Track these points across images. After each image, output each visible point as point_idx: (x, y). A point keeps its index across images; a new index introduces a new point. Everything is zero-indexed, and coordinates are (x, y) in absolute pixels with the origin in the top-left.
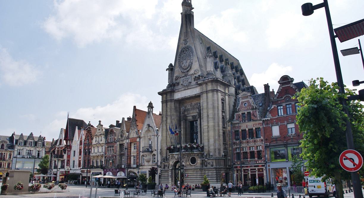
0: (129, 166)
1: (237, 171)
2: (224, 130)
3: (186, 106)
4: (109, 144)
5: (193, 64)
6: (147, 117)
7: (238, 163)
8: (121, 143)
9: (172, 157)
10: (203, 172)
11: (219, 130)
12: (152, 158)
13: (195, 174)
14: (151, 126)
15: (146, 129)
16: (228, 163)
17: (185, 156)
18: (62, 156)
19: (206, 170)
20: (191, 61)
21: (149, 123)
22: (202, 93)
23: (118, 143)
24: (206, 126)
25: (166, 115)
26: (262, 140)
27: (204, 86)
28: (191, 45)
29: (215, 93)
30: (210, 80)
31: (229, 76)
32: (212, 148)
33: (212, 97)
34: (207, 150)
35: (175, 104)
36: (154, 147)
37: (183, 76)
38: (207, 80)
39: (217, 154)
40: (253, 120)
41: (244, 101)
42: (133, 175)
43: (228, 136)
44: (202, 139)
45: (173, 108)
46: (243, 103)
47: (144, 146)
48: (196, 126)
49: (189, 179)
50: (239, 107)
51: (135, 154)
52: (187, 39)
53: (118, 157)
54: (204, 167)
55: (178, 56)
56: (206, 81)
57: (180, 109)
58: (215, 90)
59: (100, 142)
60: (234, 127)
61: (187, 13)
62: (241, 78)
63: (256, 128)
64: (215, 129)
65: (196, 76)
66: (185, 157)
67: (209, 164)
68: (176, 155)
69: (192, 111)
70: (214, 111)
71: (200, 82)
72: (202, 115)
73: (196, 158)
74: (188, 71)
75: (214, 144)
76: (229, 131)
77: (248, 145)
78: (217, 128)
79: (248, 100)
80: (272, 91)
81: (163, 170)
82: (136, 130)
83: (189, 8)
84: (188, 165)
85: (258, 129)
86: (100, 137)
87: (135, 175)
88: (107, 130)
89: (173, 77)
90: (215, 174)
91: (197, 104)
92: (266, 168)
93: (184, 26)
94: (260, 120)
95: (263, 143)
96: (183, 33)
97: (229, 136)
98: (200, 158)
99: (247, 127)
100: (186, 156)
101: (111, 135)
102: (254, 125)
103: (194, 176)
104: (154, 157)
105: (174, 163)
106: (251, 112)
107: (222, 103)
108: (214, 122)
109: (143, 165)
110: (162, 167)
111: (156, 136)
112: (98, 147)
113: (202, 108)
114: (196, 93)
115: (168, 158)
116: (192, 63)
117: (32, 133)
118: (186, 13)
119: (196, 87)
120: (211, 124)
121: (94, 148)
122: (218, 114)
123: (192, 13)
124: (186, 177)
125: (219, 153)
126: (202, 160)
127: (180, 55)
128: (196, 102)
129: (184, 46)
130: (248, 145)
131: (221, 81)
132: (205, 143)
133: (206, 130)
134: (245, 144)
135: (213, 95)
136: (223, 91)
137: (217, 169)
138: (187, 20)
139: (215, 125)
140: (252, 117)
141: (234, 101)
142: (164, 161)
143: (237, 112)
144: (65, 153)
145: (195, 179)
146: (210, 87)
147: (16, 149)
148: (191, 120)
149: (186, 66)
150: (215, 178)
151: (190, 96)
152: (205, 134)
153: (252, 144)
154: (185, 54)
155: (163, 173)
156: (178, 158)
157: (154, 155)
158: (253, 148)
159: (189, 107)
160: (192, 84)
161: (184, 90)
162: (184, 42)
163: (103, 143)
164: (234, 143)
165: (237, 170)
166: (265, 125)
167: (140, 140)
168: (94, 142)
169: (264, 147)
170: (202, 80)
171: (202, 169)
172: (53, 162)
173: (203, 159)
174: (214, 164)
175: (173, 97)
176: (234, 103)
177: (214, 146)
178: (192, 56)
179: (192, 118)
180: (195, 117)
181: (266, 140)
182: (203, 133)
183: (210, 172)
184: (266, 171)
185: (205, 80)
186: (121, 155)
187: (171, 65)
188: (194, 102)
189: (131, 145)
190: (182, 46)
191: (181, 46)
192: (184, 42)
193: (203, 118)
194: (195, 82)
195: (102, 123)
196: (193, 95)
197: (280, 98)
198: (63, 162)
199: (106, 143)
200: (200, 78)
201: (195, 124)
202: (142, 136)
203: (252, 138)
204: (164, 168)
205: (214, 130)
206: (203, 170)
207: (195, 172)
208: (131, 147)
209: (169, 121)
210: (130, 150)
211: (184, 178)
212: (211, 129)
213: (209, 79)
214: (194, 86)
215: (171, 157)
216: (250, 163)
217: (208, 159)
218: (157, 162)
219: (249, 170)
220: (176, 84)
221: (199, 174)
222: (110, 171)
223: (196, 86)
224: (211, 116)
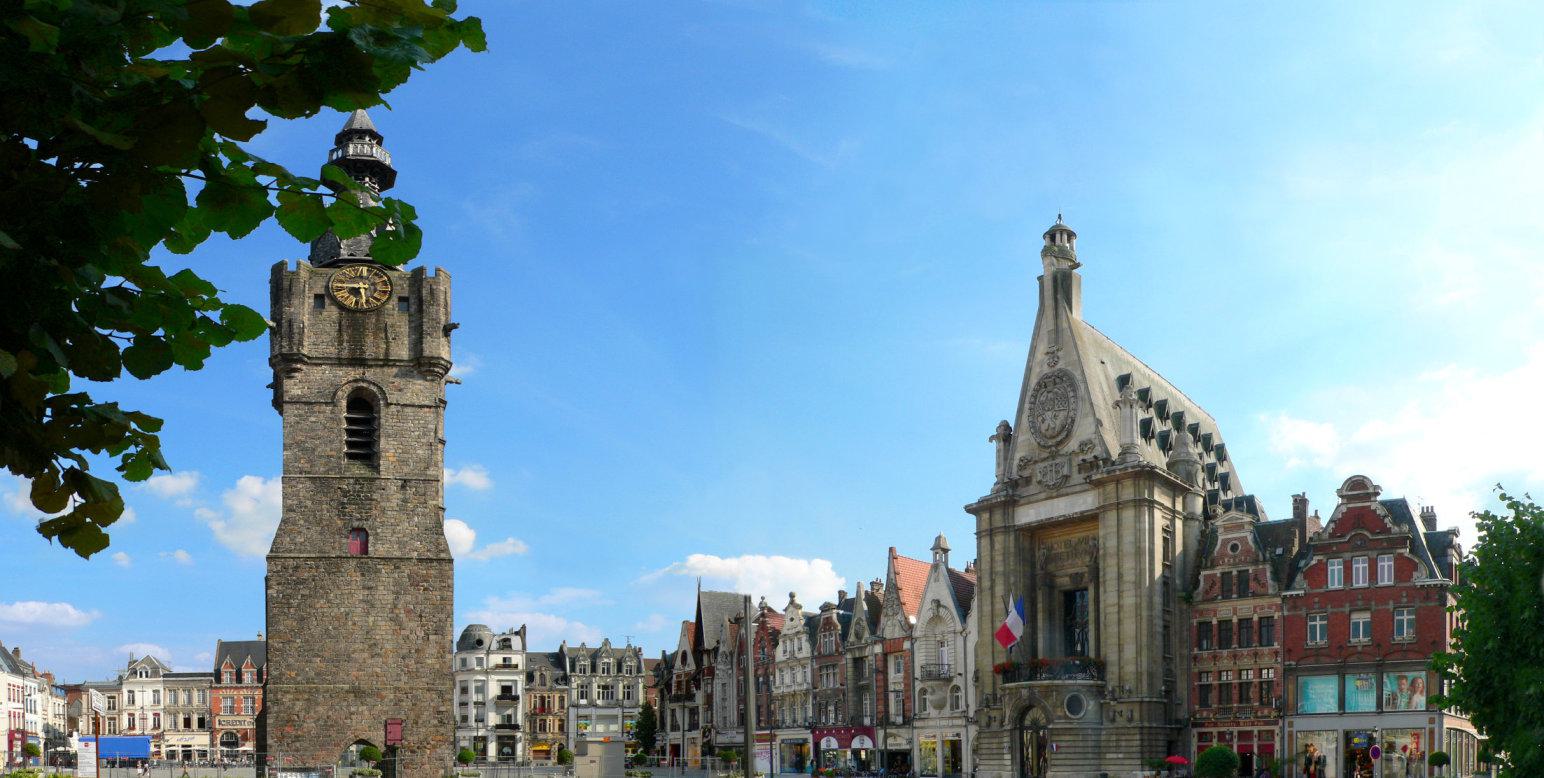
0: (885, 721)
2: (1167, 617)
3: (1052, 547)
4: (823, 661)
8: (857, 656)
12: (951, 697)
13: (1081, 744)
17: (1052, 691)
18: (691, 697)
20: (1071, 414)
22: (1103, 508)
23: (849, 656)
26: (1276, 653)
27: (1111, 488)
28: (1069, 368)
30: (1130, 470)
32: (1130, 669)
35: (1017, 539)
37: (1045, 455)
38: (1120, 470)
40: (1255, 595)
41: (1229, 536)
44: (1102, 644)
45: (1012, 550)
48: (1082, 605)
49: (1063, 756)
51: (901, 687)
52: (1058, 350)
53: (850, 694)
55: (1027, 400)
56: (1118, 473)
57: (1033, 556)
59: (797, 655)
62: (1220, 470)
63: (1260, 619)
65: (1086, 457)
69: (1070, 562)
71: (1099, 476)
72: (1101, 574)
79: (1242, 535)
80: (1313, 515)
84: (1060, 718)
85: (1266, 622)
86: (796, 640)
88: (811, 621)
89: (1012, 459)
91: (1086, 540)
92: (1282, 729)
94: (1275, 596)
95: (1279, 660)
96: (1044, 332)
99: (1235, 613)
101: (827, 633)
102: (1255, 608)
106: (1251, 571)
107: (1165, 539)
110: (984, 723)
111: (961, 633)
112: (792, 669)
113: (1101, 552)
114: (1083, 508)
115: (998, 696)
116: (1073, 421)
117: (607, 639)
120: (1129, 600)
121: (781, 670)
122: (1152, 571)
125: (1151, 685)
126: (1102, 705)
128: (1084, 534)
129: (1046, 370)
132: (1111, 654)
133: (1113, 618)
135: (1140, 517)
136: (1168, 504)
138: (1059, 296)
140: (1252, 584)
141: (1199, 538)
142: (988, 706)
144: (698, 687)
146: (1128, 492)
147: (574, 685)
148: (1068, 588)
150: (1138, 749)
152: (1110, 630)
153: (1247, 662)
154: (1050, 395)
157: (957, 689)
160: (1072, 482)
161: (1046, 499)
162: (1047, 357)
163: (805, 658)
166: (1288, 611)
167: (912, 644)
168: (779, 654)
169: (1281, 671)
170: (1104, 470)
172: (668, 713)
174: (1136, 715)
175: (1013, 517)
178: (1072, 400)
181: (1288, 652)
184: (1283, 738)
185: (1114, 471)
186: (860, 691)
187: (1005, 426)
188: (1077, 535)
189: (885, 661)
191: (1036, 370)
192: (1047, 357)
193: (1104, 582)
194: (1084, 475)
195: (798, 600)
197: (1339, 537)
198: (694, 712)
199: (813, 657)
201: (1078, 600)
203: (1249, 645)
205: (1138, 616)
207: (1080, 738)
213: (1126, 468)
214: (1078, 488)
218: (964, 708)
220: (1020, 482)
222: (830, 733)
223: (1086, 487)
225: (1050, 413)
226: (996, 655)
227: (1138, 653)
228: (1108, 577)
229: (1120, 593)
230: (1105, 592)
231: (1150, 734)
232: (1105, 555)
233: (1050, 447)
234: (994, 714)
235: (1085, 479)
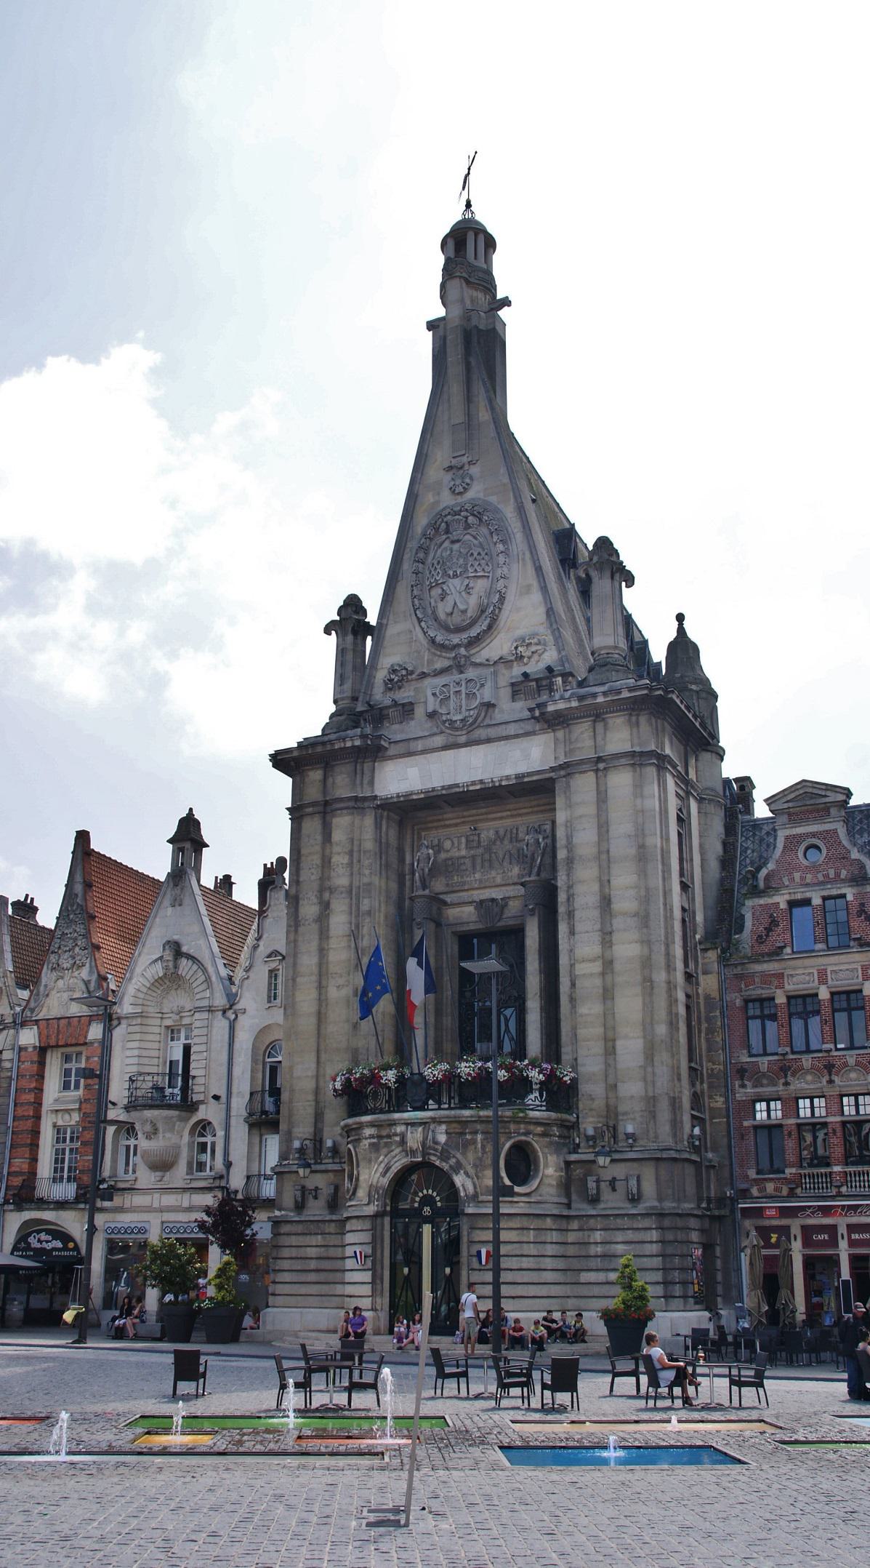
1: (764, 1232)
5: (507, 606)
6: (167, 902)
7: (770, 1187)
9: (380, 1137)
10: (571, 1237)
11: (671, 986)
12: (191, 1145)
13: (532, 1250)
14: (192, 952)
15: (158, 970)
16: (708, 1187)
17: (476, 1133)
19: (592, 1222)
21: (176, 937)
22: (568, 769)
24: (593, 960)
25: (324, 887)
27: (582, 731)
29: (651, 772)
30: (625, 694)
31: (697, 692)
32: (632, 1089)
33: (635, 797)
34: (599, 1103)
35: (378, 826)
36: (208, 1077)
37: (439, 664)
39: (665, 1129)
42: (49, 1246)
43: (704, 1025)
45: (369, 845)
46: (799, 843)
47: (134, 1069)
50: (771, 866)
54: (581, 1207)
56: (600, 699)
58: (652, 754)
60: (740, 977)
61: (474, 322)
64: (651, 981)
65: (528, 669)
66: (474, 1142)
67: (614, 1189)
68: (413, 1124)
69: (477, 876)
70: (643, 873)
72: (562, 897)
73: (534, 1151)
74: (474, 642)
75: (644, 1068)
76: (707, 997)
77: (831, 1082)
78: (660, 977)
81: (292, 1216)
82: (84, 973)
83: (480, 295)
87: (65, 1248)
90: (654, 1248)
93: (455, 389)
97: (710, 1031)
98: (557, 1148)
100: (479, 1137)
103: (526, 1263)
104: (202, 1140)
105: (390, 1175)
106: (850, 897)
108: (647, 942)
109: (121, 1185)
111: (224, 1012)
113: (561, 854)
114: (522, 768)
116: (502, 599)
118: (469, 319)
119: (527, 734)
120: (627, 949)
123: (498, 328)
124: (476, 1265)
125: (675, 1124)
126: (568, 1164)
127: (424, 549)
129: (447, 500)
130: (831, 1082)
131: (683, 707)
134: (809, 1078)
137: (667, 1222)
138: (472, 360)
139: (649, 958)
143: (756, 892)
145: (533, 1277)
148: (472, 927)
149: (464, 612)
151: (481, 782)
152: (583, 1010)
154: (456, 546)
155: (294, 1240)
156: (424, 1144)
157: (204, 1126)
158: (857, 1105)
159: (456, 848)
160: (498, 716)
161: (446, 748)
162: (449, 476)
164: (742, 1072)
165: (757, 1228)
171: (568, 1217)
173: (573, 1157)
174: (649, 1188)
175: (372, 783)
176: (725, 844)
177: (645, 1080)
179: (474, 918)
180: (496, 909)
182: (572, 1000)
183: (620, 1239)
187: (353, 605)
189: (42, 1064)
190: (437, 502)
196: (508, 778)
200: (551, 684)
202: (126, 1007)
204: (300, 1206)
205: (648, 984)
206: (575, 1225)
207: (531, 1236)
208: (41, 1076)
209: (339, 921)
210: (39, 1090)
211: (464, 1273)
212: (627, 976)
214: (512, 729)
215: (372, 1137)
216: (844, 1189)
217: (314, 1167)
219: (842, 1230)
221: (550, 1250)
223: (528, 726)
224: (625, 902)
225: (457, 582)
226: (323, 1056)
227: (650, 1053)
228: (579, 902)
229: (607, 937)
230: (572, 932)
231: (827, 1188)
232: (570, 861)
233: (458, 646)
234: (320, 1181)
235: (531, 710)
